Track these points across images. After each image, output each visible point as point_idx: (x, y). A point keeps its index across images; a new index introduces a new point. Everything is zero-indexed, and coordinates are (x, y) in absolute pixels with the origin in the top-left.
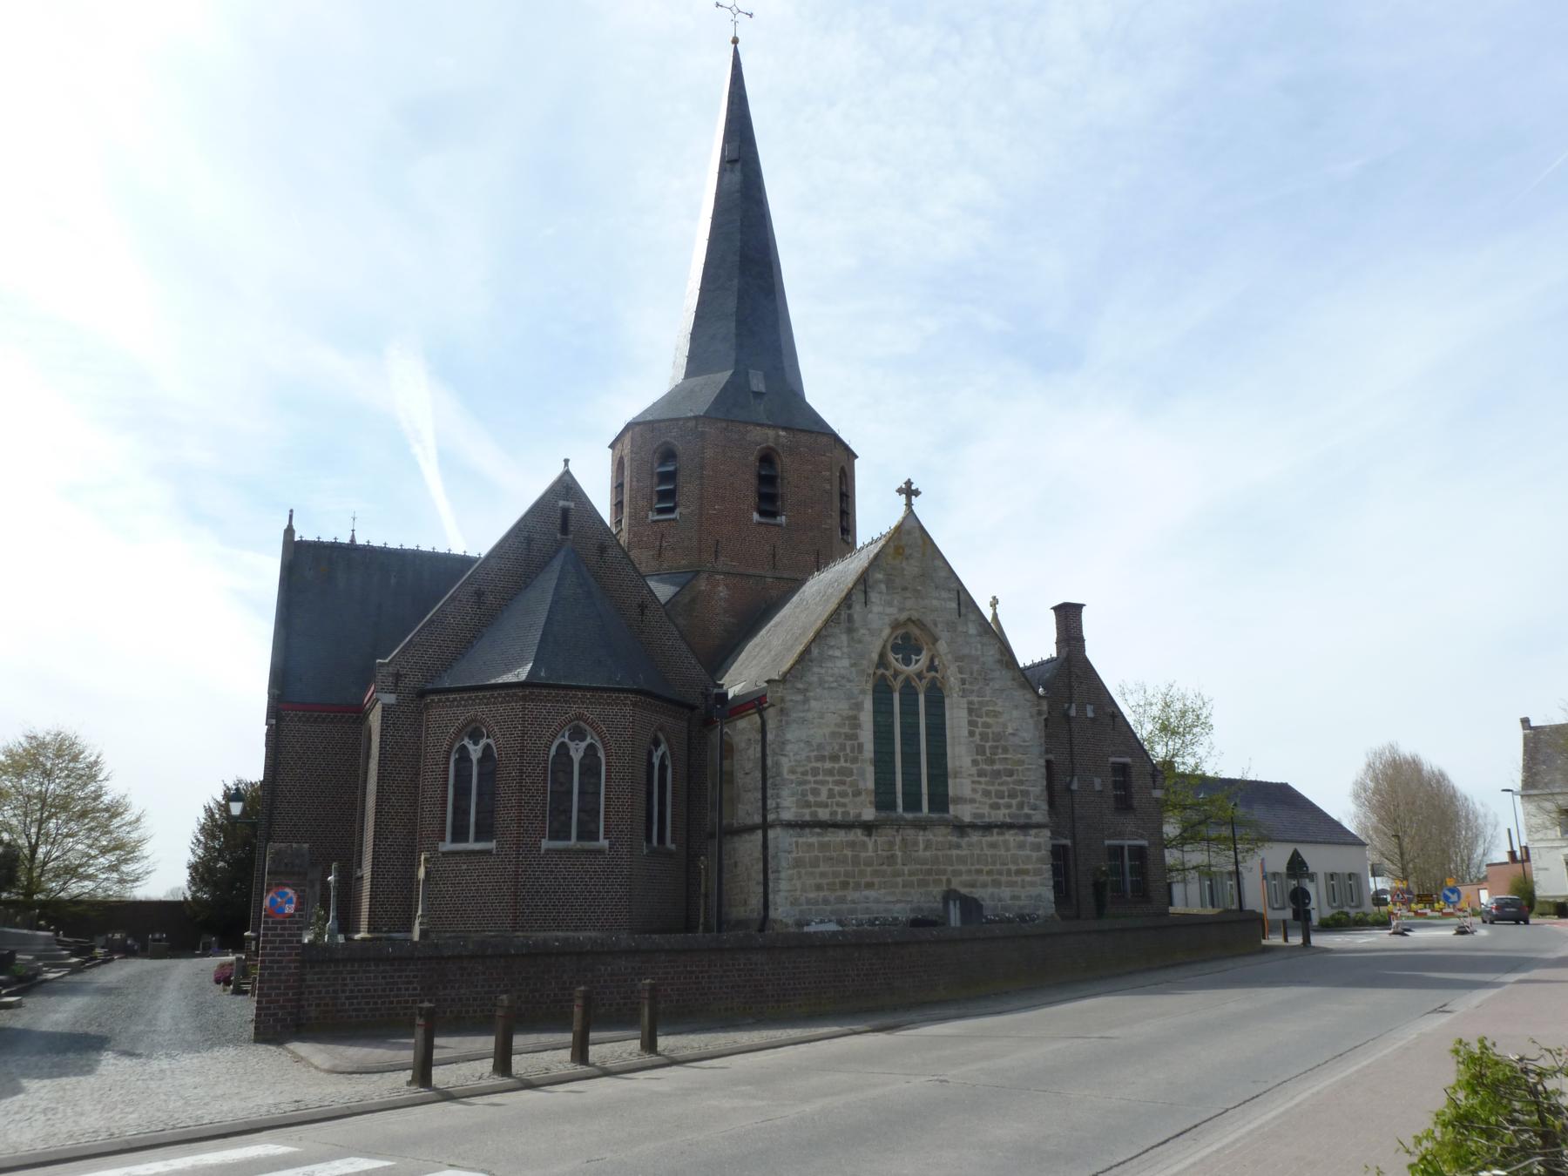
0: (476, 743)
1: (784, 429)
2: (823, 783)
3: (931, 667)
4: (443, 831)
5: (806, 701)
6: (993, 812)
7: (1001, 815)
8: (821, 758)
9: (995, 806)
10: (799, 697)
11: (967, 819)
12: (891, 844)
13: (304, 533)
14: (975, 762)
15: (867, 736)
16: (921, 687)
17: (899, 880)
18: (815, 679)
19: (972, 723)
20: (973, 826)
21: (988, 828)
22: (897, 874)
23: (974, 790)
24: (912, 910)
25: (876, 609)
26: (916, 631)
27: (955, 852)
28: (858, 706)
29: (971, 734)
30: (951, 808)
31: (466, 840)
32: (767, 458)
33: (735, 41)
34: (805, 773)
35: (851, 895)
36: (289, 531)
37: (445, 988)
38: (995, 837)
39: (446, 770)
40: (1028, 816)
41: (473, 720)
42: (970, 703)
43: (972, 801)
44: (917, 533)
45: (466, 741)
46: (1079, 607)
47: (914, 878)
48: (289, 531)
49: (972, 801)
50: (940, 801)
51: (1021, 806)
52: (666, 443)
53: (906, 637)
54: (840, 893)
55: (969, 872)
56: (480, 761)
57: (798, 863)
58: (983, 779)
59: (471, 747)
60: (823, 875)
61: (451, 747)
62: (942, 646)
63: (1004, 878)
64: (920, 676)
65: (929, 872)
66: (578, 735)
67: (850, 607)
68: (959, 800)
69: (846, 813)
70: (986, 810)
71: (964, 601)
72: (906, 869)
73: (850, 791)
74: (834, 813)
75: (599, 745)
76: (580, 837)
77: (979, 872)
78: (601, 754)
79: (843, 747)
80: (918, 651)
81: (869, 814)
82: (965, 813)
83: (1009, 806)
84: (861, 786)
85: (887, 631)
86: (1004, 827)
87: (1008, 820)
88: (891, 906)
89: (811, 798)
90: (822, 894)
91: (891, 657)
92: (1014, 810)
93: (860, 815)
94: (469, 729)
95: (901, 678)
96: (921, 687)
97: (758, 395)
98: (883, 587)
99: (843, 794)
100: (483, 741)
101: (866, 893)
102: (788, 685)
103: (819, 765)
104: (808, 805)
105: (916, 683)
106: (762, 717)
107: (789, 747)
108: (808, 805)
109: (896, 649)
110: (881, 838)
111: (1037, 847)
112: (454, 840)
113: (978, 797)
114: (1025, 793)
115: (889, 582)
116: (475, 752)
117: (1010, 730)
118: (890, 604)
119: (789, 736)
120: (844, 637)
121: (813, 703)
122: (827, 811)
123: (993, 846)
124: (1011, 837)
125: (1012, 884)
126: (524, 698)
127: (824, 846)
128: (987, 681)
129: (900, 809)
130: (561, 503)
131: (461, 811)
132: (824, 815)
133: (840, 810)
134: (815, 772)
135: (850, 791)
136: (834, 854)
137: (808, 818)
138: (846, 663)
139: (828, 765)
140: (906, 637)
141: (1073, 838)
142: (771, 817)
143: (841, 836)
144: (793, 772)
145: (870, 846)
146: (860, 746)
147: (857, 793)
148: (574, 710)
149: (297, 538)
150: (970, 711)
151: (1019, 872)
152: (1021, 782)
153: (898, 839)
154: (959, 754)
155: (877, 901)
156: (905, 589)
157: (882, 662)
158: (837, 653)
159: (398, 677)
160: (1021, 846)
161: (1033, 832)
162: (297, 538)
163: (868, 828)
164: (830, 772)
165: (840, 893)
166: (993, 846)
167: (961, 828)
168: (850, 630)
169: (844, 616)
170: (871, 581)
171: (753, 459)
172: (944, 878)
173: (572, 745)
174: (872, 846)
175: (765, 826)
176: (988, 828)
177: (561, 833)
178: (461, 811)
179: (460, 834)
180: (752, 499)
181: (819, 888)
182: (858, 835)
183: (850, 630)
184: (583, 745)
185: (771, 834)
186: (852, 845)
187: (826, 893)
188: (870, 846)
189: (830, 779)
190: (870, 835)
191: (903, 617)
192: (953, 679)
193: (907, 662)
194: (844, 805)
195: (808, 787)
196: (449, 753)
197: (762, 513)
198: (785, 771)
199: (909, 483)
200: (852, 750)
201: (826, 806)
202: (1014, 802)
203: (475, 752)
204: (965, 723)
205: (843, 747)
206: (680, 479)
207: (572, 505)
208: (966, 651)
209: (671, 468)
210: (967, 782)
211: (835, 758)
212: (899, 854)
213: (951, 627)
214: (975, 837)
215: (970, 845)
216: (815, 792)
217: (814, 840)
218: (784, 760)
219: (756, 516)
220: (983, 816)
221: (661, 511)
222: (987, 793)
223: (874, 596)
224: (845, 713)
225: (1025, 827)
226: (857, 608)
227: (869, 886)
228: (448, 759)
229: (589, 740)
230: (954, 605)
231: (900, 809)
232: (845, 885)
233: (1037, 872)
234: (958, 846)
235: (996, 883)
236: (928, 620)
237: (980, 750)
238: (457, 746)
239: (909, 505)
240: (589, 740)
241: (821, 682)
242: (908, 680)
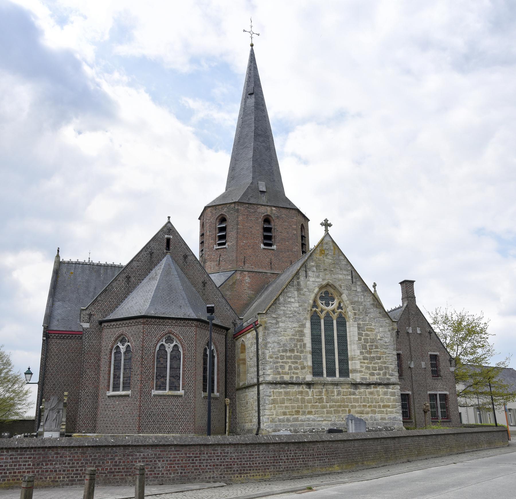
0: (123, 345)
1: (274, 207)
2: (286, 363)
3: (339, 307)
4: (109, 386)
5: (277, 323)
6: (371, 377)
7: (375, 379)
8: (285, 351)
9: (372, 374)
10: (274, 321)
11: (358, 380)
12: (321, 392)
13: (65, 257)
14: (362, 353)
15: (308, 340)
16: (335, 317)
17: (325, 410)
18: (282, 312)
19: (359, 334)
20: (362, 384)
21: (369, 385)
22: (323, 407)
23: (362, 367)
24: (332, 425)
25: (311, 279)
26: (331, 290)
27: (352, 397)
28: (303, 326)
29: (360, 339)
30: (350, 375)
31: (119, 390)
32: (267, 220)
33: (58, 251)
34: (277, 358)
35: (301, 417)
36: (58, 256)
37: (47, 465)
38: (372, 389)
39: (110, 357)
40: (388, 379)
41: (122, 334)
42: (359, 324)
43: (361, 372)
44: (331, 244)
45: (119, 344)
46: (412, 282)
47: (332, 409)
48: (58, 256)
49: (361, 372)
50: (345, 372)
51: (385, 374)
52: (222, 214)
53: (327, 293)
54: (295, 416)
55: (360, 406)
56: (125, 353)
57: (274, 402)
58: (366, 361)
59: (121, 347)
60: (286, 407)
61: (112, 347)
62: (344, 297)
63: (377, 410)
64: (333, 311)
65: (340, 406)
66: (169, 340)
67: (298, 278)
68: (355, 371)
69: (298, 377)
70: (368, 376)
71: (355, 276)
72: (328, 404)
73: (299, 367)
74: (292, 377)
75: (179, 345)
76: (170, 389)
77: (365, 406)
78: (181, 350)
79: (296, 345)
80: (333, 299)
81: (309, 378)
82: (356, 377)
83: (379, 374)
84: (305, 364)
85: (317, 290)
86: (377, 384)
87: (379, 381)
88: (320, 423)
89: (280, 370)
90: (286, 417)
91: (319, 302)
92: (381, 376)
93: (305, 378)
94: (120, 338)
95: (324, 312)
96: (335, 317)
97: (262, 192)
98: (315, 269)
99: (296, 368)
100: (127, 344)
101: (308, 416)
102: (269, 316)
103: (284, 354)
104: (279, 373)
105: (332, 314)
106: (256, 331)
107: (269, 345)
108: (279, 373)
109: (322, 298)
110: (315, 390)
111: (393, 394)
112: (113, 391)
113: (363, 369)
114: (387, 368)
115: (318, 266)
116: (123, 349)
117: (379, 338)
118: (318, 277)
119: (269, 340)
120: (296, 293)
121: (281, 324)
122: (288, 376)
123: (371, 393)
124: (381, 390)
125: (382, 412)
126: (144, 323)
127: (287, 393)
128: (367, 313)
129: (325, 375)
130: (166, 236)
131: (116, 377)
132: (287, 378)
133: (295, 376)
134: (282, 357)
135: (299, 367)
136: (292, 398)
137: (279, 380)
138: (297, 305)
139: (288, 354)
140: (327, 293)
141: (412, 390)
142: (261, 379)
143: (296, 389)
144: (271, 357)
145: (310, 393)
146: (305, 345)
147: (303, 368)
148: (167, 329)
149: (61, 260)
150: (359, 328)
151: (384, 406)
152: (385, 363)
153: (324, 390)
154: (354, 349)
155: (314, 420)
156: (325, 270)
157: (315, 305)
158: (293, 300)
159: (90, 315)
160: (385, 394)
161: (391, 387)
162: (61, 260)
163: (309, 385)
164: (290, 357)
165: (295, 416)
166: (371, 393)
167: (355, 385)
168: (299, 290)
169: (295, 283)
170: (308, 267)
171: (261, 220)
172: (347, 409)
173: (166, 345)
174: (311, 393)
175: (258, 384)
176: (369, 385)
177: (161, 386)
178: (116, 377)
179: (116, 388)
180: (261, 238)
181: (285, 414)
182: (305, 388)
183: (299, 290)
184: (172, 345)
185: (261, 387)
186: (301, 393)
187: (289, 416)
188: (310, 393)
189: (290, 361)
190: (310, 388)
191: (324, 283)
192: (350, 313)
193: (327, 305)
194: (297, 373)
195: (278, 365)
196: (111, 350)
197: (265, 244)
198: (267, 357)
199: (326, 220)
200: (301, 347)
201: (288, 374)
202: (381, 372)
203: (123, 349)
204: (356, 334)
205: (296, 345)
206: (228, 229)
207: (171, 237)
208: (356, 299)
209: (224, 225)
210: (358, 362)
211: (292, 351)
212: (325, 397)
213: (349, 288)
214: (362, 389)
215: (360, 393)
216: (282, 367)
217: (282, 390)
218: (267, 351)
219: (262, 246)
220: (366, 379)
221: (220, 244)
222: (368, 368)
223: (310, 273)
224: (297, 329)
225: (387, 385)
226: (302, 278)
227: (310, 413)
228: (111, 352)
229: (175, 343)
230: (350, 278)
231: (325, 375)
232: (298, 412)
233: (394, 407)
234: (354, 394)
235: (374, 412)
236: (337, 285)
237: (364, 347)
238: (115, 346)
239: (326, 230)
240: (175, 343)
241: (285, 315)
242: (328, 313)
